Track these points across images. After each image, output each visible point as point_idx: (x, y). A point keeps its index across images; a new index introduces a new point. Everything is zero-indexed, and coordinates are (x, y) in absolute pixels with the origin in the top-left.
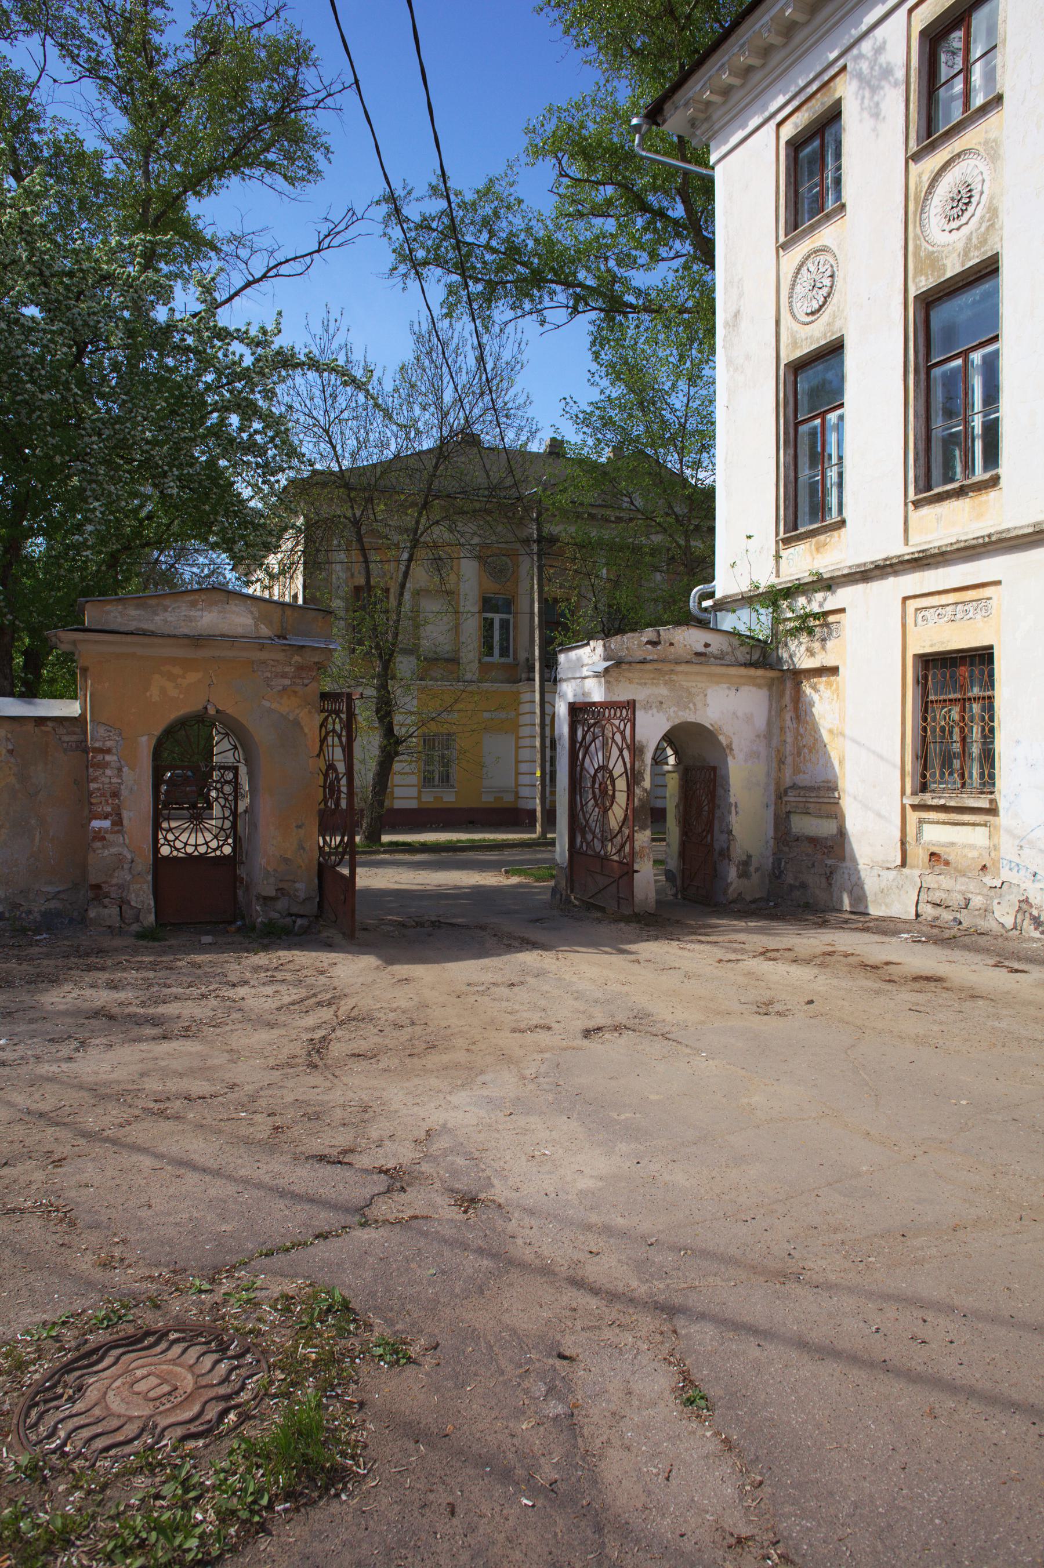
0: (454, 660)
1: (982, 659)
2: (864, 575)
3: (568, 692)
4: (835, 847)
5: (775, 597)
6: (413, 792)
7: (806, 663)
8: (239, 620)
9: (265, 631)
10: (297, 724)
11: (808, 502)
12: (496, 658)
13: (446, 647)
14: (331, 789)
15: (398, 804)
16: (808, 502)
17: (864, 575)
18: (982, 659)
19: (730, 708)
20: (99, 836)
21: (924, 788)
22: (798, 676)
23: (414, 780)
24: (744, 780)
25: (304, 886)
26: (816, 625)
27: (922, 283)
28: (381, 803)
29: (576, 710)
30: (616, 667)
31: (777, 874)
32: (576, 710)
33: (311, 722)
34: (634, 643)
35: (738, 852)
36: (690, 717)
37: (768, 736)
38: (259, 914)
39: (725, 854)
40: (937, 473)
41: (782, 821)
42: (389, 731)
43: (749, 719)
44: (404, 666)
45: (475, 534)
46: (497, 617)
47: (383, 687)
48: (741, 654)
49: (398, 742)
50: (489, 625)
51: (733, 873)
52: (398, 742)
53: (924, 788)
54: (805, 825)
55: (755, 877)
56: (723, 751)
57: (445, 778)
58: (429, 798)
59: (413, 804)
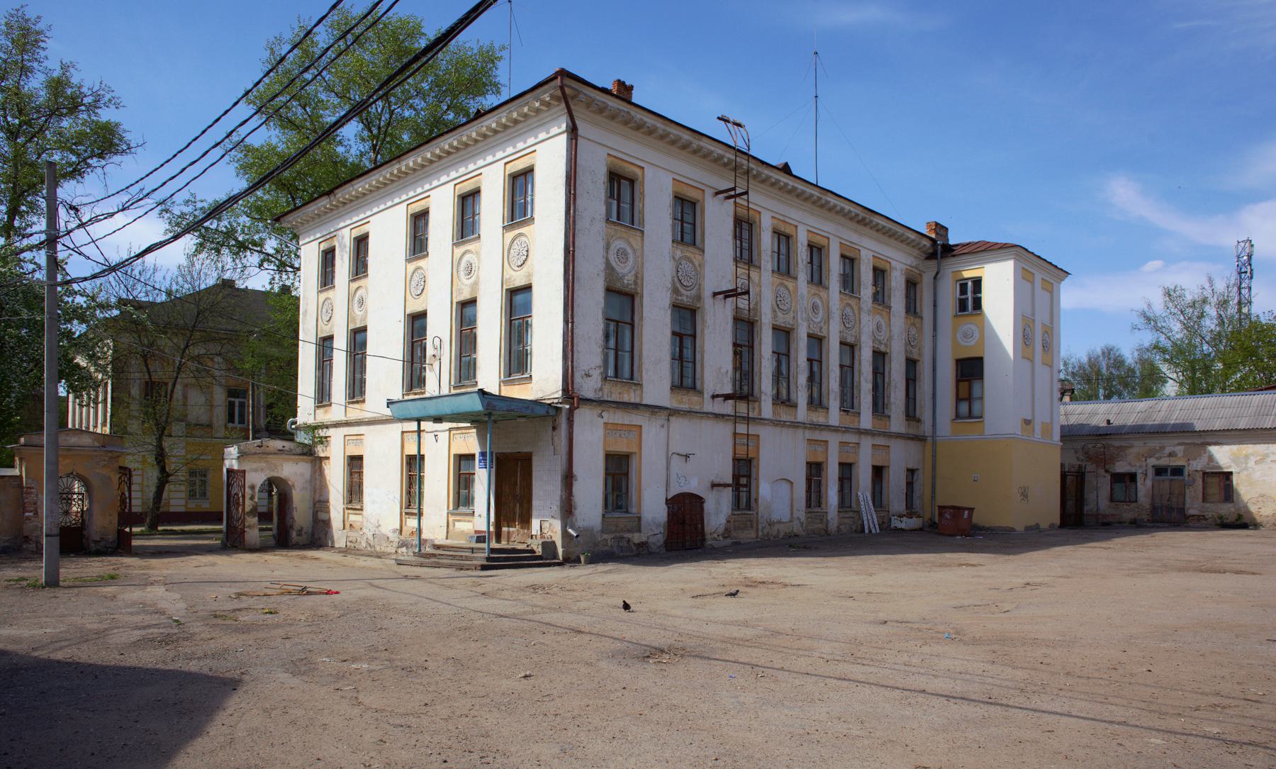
0: (210, 426)
1: (360, 458)
2: (337, 425)
3: (227, 464)
4: (327, 523)
5: (313, 428)
6: (183, 502)
7: (322, 455)
8: (86, 440)
9: (96, 444)
10: (109, 478)
11: (323, 396)
12: (237, 424)
13: (204, 419)
14: (123, 501)
15: (172, 509)
16: (323, 396)
17: (337, 425)
18: (360, 458)
19: (293, 471)
20: (28, 518)
21: (350, 502)
22: (321, 459)
23: (183, 495)
24: (299, 498)
25: (112, 537)
26: (324, 441)
27: (352, 326)
28: (158, 508)
29: (229, 471)
30: (242, 456)
31: (313, 534)
32: (229, 471)
33: (115, 478)
34: (252, 444)
35: (296, 526)
36: (275, 474)
37: (311, 481)
38: (93, 547)
39: (291, 527)
40: (357, 391)
41: (315, 514)
42: (163, 470)
43: (302, 475)
44: (177, 428)
45: (379, 128)
46: (237, 401)
47: (160, 439)
48: (299, 450)
49: (169, 475)
50: (231, 405)
51: (294, 534)
52: (169, 475)
53: (350, 502)
54: (322, 516)
55: (305, 536)
56: (290, 487)
57: (204, 494)
58: (193, 506)
59: (182, 509)
